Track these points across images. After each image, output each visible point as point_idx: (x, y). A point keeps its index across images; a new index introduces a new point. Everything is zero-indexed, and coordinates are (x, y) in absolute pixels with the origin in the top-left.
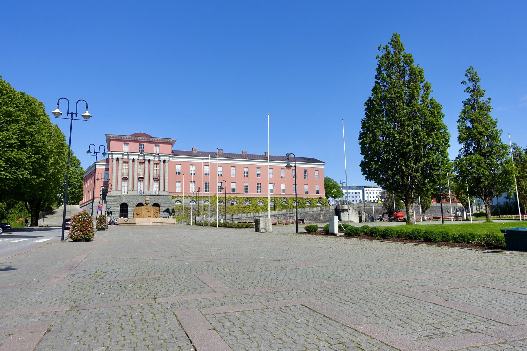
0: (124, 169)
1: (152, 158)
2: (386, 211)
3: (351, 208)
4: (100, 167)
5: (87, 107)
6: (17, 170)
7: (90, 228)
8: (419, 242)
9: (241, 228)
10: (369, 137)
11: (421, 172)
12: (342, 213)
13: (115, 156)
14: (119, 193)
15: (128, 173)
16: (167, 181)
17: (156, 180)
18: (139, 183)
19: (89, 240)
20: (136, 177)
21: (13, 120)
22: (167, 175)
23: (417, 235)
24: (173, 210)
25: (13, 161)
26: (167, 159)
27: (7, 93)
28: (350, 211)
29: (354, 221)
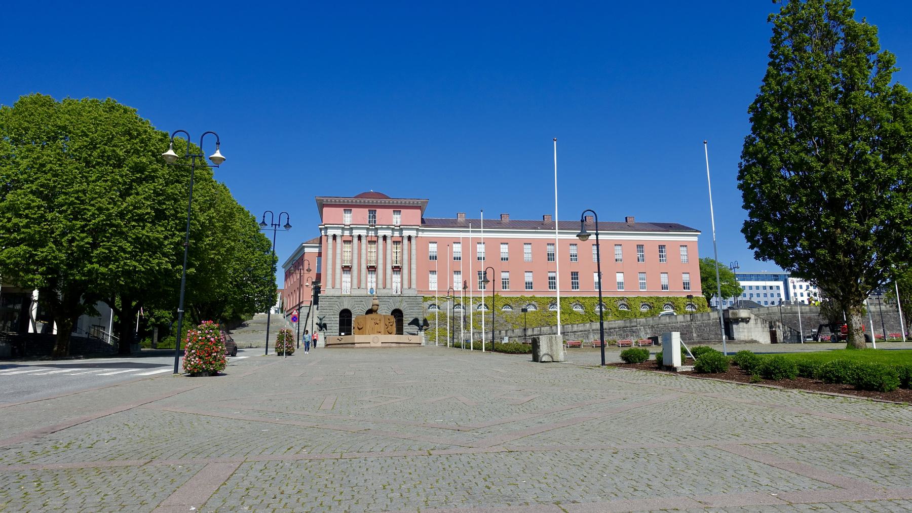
0: (346, 253)
1: (388, 233)
2: (826, 322)
3: (753, 317)
4: (311, 251)
5: (218, 144)
6: (150, 256)
7: (217, 352)
8: (841, 391)
9: (521, 353)
10: (756, 173)
11: (875, 238)
12: (735, 326)
13: (331, 232)
14: (338, 293)
15: (352, 260)
16: (414, 271)
17: (397, 269)
18: (369, 276)
19: (215, 374)
20: (364, 267)
21: (147, 177)
22: (414, 261)
23: (842, 373)
24: (425, 321)
25: (144, 241)
26: (413, 233)
27: (139, 134)
28: (752, 322)
29: (761, 340)
